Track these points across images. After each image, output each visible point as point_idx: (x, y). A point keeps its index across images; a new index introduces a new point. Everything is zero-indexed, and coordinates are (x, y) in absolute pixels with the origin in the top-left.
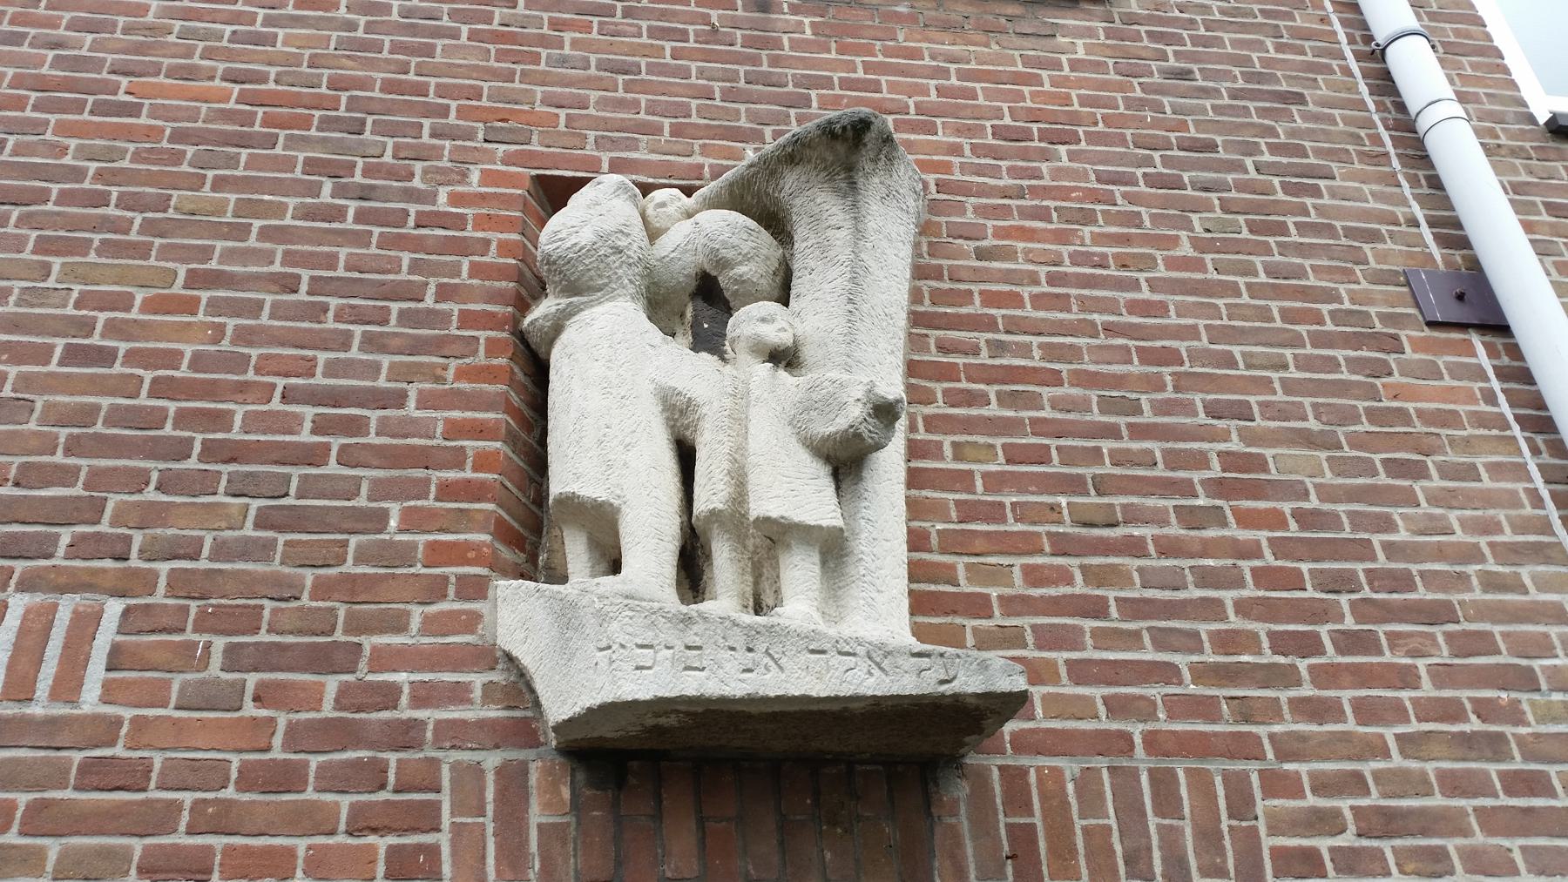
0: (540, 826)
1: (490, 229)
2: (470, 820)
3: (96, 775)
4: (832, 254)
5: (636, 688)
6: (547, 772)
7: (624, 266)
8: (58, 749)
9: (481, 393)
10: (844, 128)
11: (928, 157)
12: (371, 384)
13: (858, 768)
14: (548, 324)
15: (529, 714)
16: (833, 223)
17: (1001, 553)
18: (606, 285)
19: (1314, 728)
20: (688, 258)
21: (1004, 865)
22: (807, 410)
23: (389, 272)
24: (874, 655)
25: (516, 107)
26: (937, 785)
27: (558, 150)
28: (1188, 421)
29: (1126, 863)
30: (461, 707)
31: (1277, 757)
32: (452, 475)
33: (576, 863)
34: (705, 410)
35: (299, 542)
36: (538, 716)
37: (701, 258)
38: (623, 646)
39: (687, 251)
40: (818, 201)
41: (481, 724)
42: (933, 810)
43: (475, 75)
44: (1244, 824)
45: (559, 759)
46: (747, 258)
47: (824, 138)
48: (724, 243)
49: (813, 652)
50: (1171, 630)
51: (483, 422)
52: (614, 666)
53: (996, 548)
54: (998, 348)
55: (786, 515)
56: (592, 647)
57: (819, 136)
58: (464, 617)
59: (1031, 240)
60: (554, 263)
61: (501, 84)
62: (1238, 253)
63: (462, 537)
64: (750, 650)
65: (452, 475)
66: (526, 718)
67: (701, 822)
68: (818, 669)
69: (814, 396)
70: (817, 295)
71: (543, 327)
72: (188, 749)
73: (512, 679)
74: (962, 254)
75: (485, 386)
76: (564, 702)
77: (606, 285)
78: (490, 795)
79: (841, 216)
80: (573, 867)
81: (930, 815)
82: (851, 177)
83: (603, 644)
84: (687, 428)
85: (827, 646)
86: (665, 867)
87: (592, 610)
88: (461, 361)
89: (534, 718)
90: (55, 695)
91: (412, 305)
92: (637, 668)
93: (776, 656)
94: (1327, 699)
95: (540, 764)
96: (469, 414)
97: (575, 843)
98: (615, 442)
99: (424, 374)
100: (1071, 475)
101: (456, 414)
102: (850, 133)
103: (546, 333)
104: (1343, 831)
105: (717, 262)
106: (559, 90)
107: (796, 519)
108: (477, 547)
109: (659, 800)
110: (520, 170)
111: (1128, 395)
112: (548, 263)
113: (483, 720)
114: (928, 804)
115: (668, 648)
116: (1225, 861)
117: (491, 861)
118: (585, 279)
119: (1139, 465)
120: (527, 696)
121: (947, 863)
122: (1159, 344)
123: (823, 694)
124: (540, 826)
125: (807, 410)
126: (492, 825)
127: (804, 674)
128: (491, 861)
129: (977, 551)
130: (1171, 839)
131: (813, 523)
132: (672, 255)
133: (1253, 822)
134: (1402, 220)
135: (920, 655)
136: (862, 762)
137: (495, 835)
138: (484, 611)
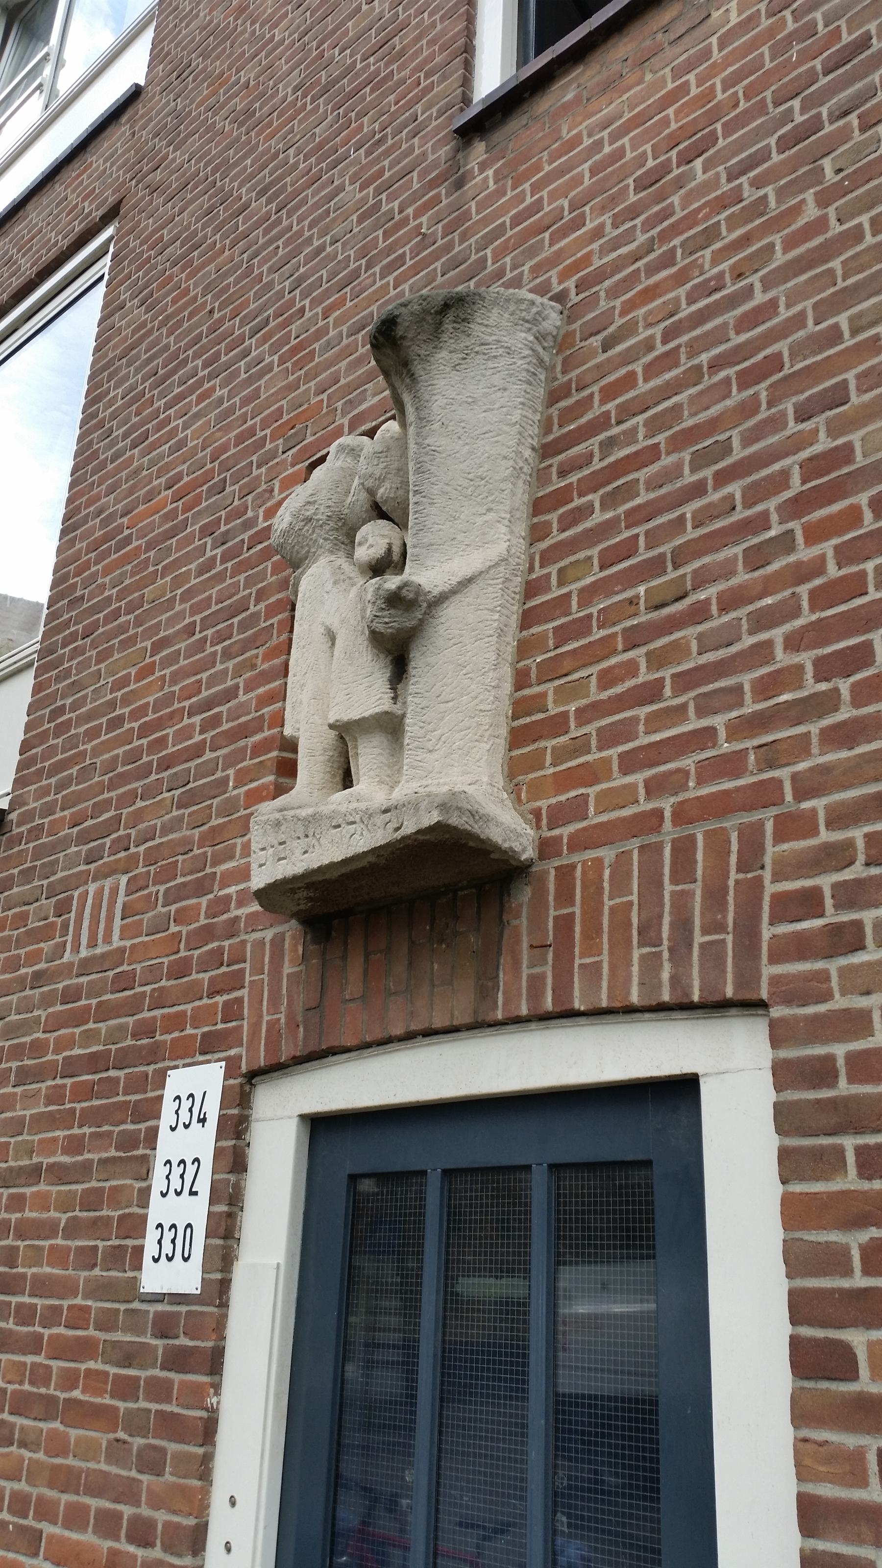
6: (293, 937)
7: (317, 531)
11: (573, 258)
12: (223, 686)
13: (460, 893)
17: (585, 666)
18: (308, 552)
19: (844, 754)
23: (234, 595)
25: (301, 409)
26: (509, 895)
29: (639, 933)
31: (795, 798)
35: (194, 812)
42: (505, 918)
44: (749, 875)
46: (381, 480)
50: (715, 691)
54: (608, 445)
55: (338, 718)
62: (868, 181)
64: (307, 836)
74: (593, 354)
77: (308, 552)
81: (501, 920)
90: (627, 854)
91: (244, 615)
94: (869, 716)
100: (653, 557)
102: (381, 339)
104: (851, 863)
107: (346, 719)
109: (346, 944)
116: (725, 917)
117: (265, 1003)
119: (717, 517)
122: (760, 356)
128: (265, 1003)
130: (682, 902)
131: (357, 718)
133: (760, 872)
136: (462, 889)
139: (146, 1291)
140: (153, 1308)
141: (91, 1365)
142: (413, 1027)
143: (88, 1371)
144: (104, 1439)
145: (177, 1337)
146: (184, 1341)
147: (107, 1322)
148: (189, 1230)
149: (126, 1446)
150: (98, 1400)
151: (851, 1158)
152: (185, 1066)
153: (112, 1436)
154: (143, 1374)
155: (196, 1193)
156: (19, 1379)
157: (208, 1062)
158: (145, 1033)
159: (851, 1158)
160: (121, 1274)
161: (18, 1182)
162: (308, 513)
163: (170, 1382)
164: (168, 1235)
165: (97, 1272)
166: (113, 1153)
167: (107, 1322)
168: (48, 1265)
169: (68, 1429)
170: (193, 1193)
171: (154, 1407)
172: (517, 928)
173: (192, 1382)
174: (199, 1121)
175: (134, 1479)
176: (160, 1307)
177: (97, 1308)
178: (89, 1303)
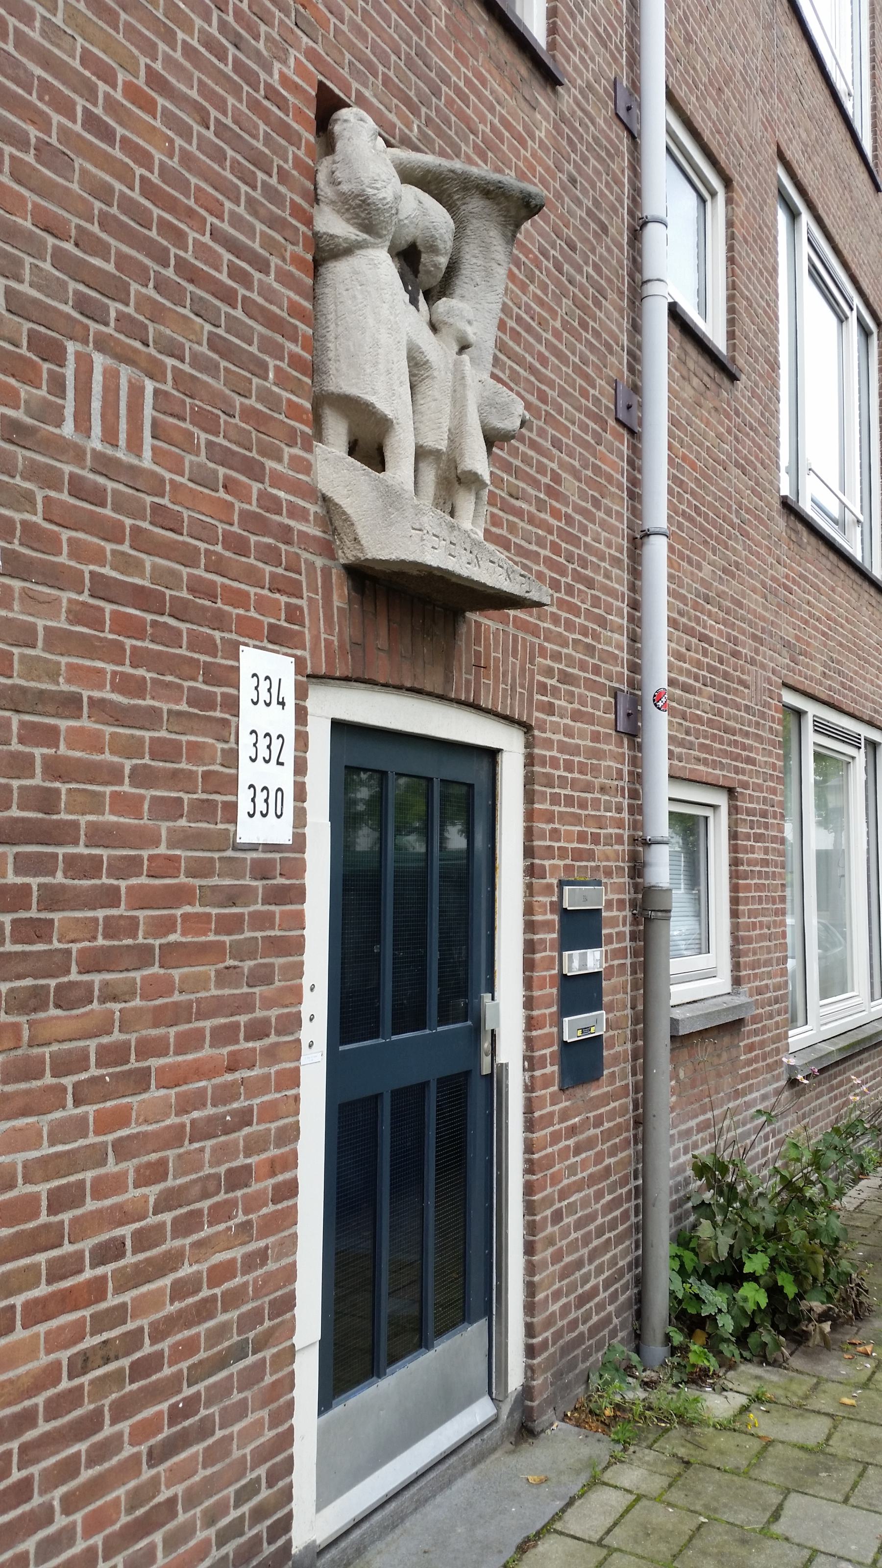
3: (159, 515)
8: (138, 490)
20: (412, 229)
27: (332, 62)
34: (436, 374)
37: (418, 233)
40: (491, 234)
49: (491, 562)
56: (409, 525)
57: (518, 198)
60: (369, 205)
67: (389, 621)
72: (200, 512)
76: (382, 549)
83: (417, 526)
105: (431, 246)
112: (363, 201)
114: (454, 634)
125: (490, 405)
134: (397, 137)
135: (522, 575)
139: (242, 841)
140: (250, 855)
141: (188, 909)
142: (391, 682)
143: (186, 917)
144: (211, 970)
145: (274, 878)
146: (280, 881)
147: (200, 869)
148: (279, 793)
149: (238, 970)
150: (203, 939)
151: (38, 770)
152: (255, 647)
153: (221, 966)
154: (245, 910)
155: (282, 764)
156: (89, 936)
157: (277, 652)
158: (204, 593)
159: (38, 770)
160: (212, 826)
161: (40, 708)
163: (273, 914)
164: (261, 796)
165: (183, 822)
166: (184, 707)
167: (200, 869)
168: (112, 812)
169: (170, 971)
170: (280, 764)
171: (259, 934)
172: (460, 646)
173: (291, 911)
174: (279, 703)
175: (247, 994)
176: (254, 855)
177: (187, 858)
178: (178, 852)
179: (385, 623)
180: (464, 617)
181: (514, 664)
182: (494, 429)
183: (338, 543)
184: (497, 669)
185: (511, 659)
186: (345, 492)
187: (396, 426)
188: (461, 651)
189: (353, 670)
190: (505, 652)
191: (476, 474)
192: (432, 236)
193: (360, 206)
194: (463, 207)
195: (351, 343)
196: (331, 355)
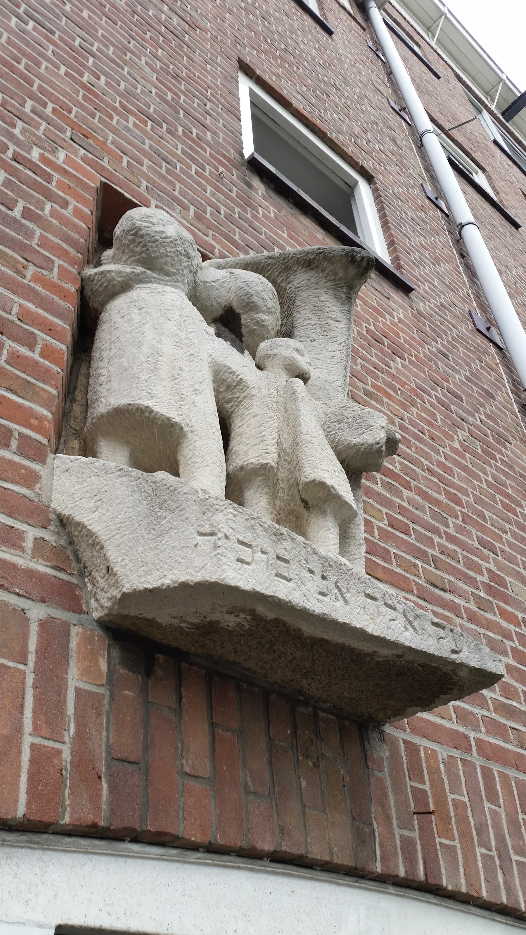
0: (77, 690)
1: (69, 194)
2: (11, 664)
4: (332, 334)
5: (238, 576)
6: (87, 640)
9: (52, 302)
10: (363, 258)
13: (321, 713)
14: (120, 279)
15: (74, 580)
16: (332, 316)
18: (174, 274)
21: (412, 820)
22: (339, 421)
24: (408, 614)
25: (94, 134)
26: (369, 743)
28: (471, 542)
30: (12, 551)
32: (23, 350)
33: (108, 737)
36: (81, 585)
38: (226, 537)
39: (223, 287)
41: (30, 574)
43: (67, 97)
45: (98, 632)
47: (344, 259)
48: (257, 292)
49: (368, 596)
51: (52, 324)
52: (220, 551)
53: (389, 579)
57: (341, 256)
58: (23, 471)
59: (390, 399)
60: (142, 236)
61: (85, 115)
63: (27, 403)
64: (324, 578)
65: (23, 350)
66: (71, 583)
67: (212, 725)
68: (371, 611)
69: (346, 413)
70: (318, 356)
71: (114, 279)
73: (62, 543)
75: (57, 299)
77: (174, 274)
78: (33, 644)
79: (340, 315)
80: (104, 740)
82: (350, 294)
83: (207, 529)
84: (229, 401)
85: (378, 596)
86: (184, 761)
87: (195, 498)
88: (39, 270)
89: (77, 586)
92: (238, 560)
93: (343, 590)
95: (81, 630)
96: (41, 311)
97: (108, 717)
98: (186, 384)
99: (8, 263)
101: (30, 306)
102: (364, 264)
103: (114, 286)
105: (248, 304)
106: (124, 143)
108: (41, 419)
110: (94, 172)
111: (442, 513)
112: (135, 234)
113: (32, 571)
115: (263, 552)
118: (162, 260)
120: (74, 564)
121: (380, 809)
123: (376, 633)
124: (77, 690)
125: (339, 421)
126: (32, 676)
127: (362, 612)
129: (379, 577)
132: (213, 284)
136: (324, 710)
137: (35, 687)
138: (42, 473)
162: (191, 251)
172: (380, 781)
179: (205, 727)
180: (382, 733)
181: (495, 814)
182: (350, 447)
183: (89, 587)
184: (462, 821)
185: (487, 805)
186: (92, 505)
187: (190, 435)
188: (384, 789)
189: (113, 812)
190: (473, 792)
191: (322, 485)
192: (247, 294)
193: (133, 241)
194: (289, 286)
195: (124, 360)
196: (102, 379)
